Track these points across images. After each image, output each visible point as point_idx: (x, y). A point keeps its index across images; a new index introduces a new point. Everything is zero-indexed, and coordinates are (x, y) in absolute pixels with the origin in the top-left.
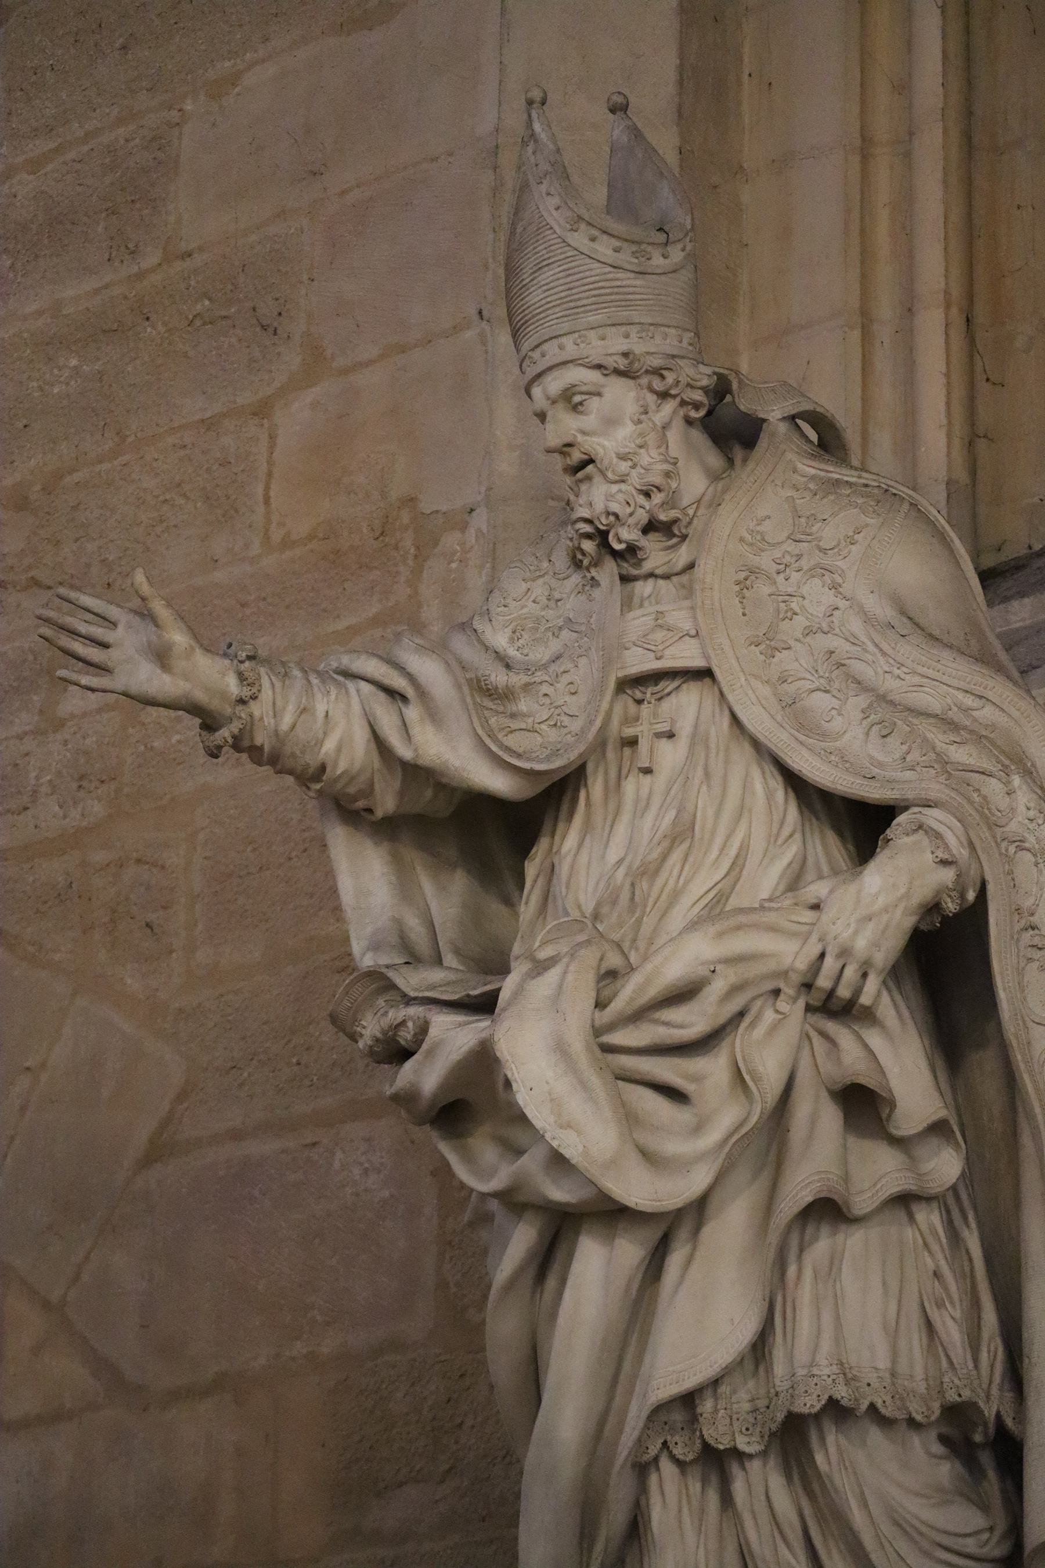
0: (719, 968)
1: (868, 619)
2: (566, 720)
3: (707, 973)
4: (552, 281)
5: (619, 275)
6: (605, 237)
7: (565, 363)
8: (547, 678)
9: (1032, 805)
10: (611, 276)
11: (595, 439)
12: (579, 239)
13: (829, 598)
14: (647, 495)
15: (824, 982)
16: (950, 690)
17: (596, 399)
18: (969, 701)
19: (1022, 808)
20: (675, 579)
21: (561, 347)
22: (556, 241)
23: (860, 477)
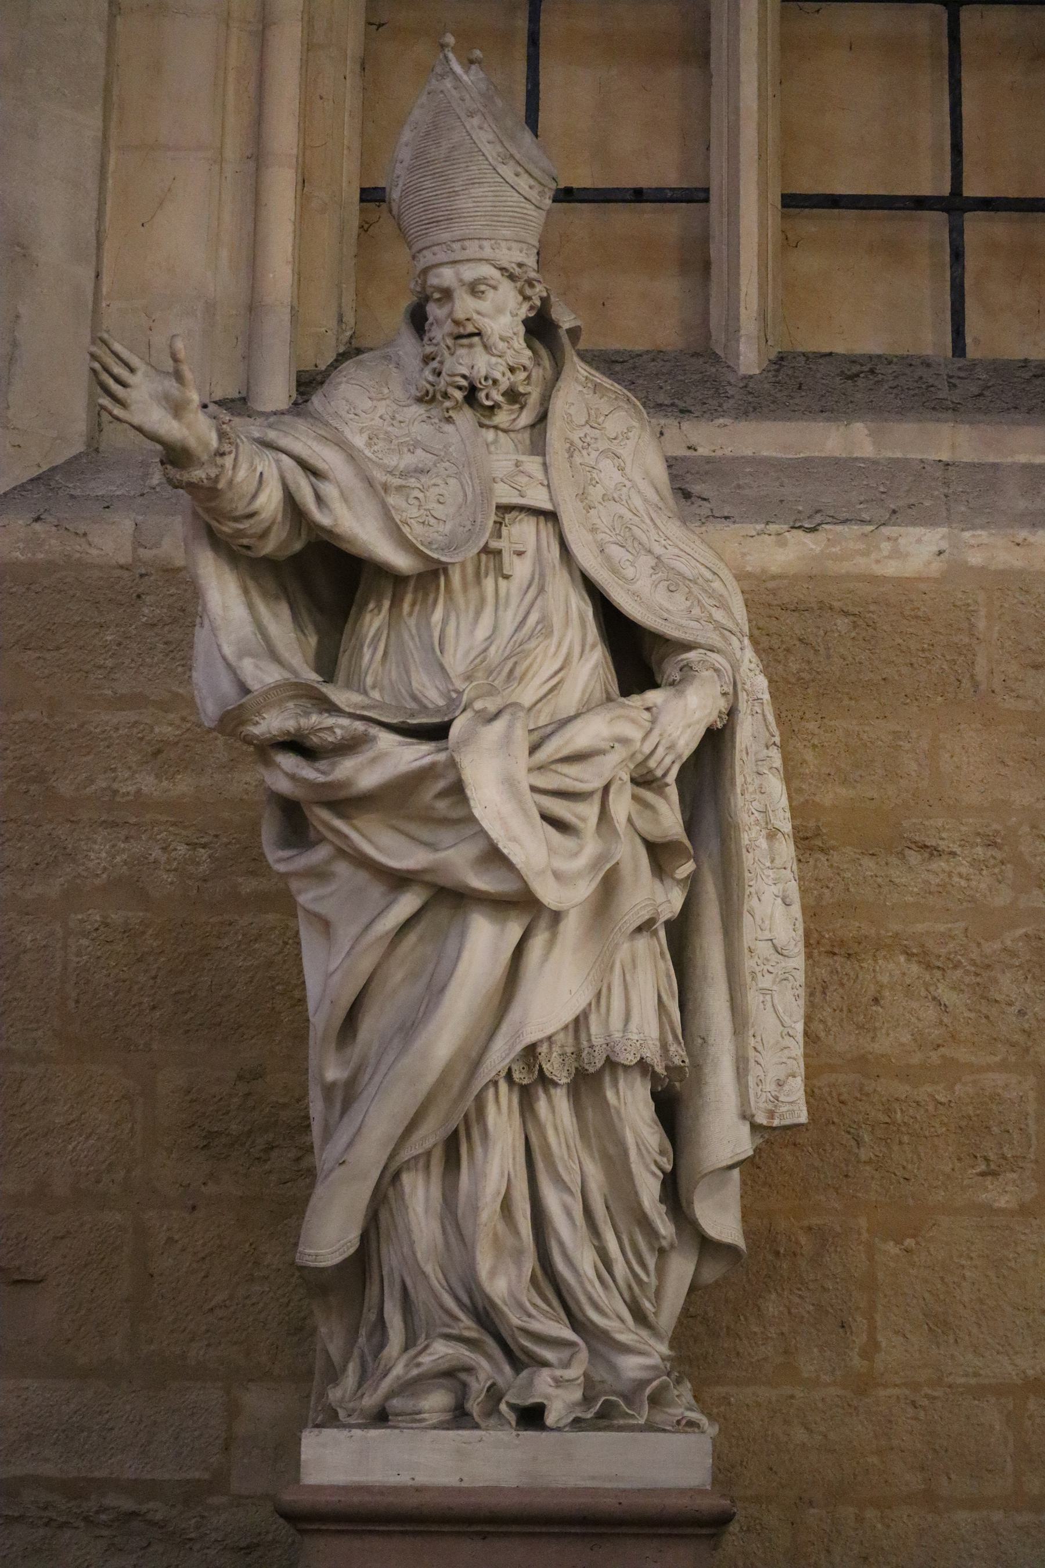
0: (616, 745)
1: (645, 500)
2: (432, 521)
3: (608, 747)
4: (482, 196)
5: (527, 206)
6: (526, 176)
7: (480, 260)
8: (418, 485)
9: (753, 660)
10: (522, 205)
11: (486, 320)
12: (507, 171)
13: (617, 476)
14: (512, 370)
15: (652, 763)
16: (698, 564)
17: (492, 291)
18: (708, 575)
19: (746, 661)
20: (512, 435)
21: (481, 247)
22: (485, 167)
23: (612, 385)
